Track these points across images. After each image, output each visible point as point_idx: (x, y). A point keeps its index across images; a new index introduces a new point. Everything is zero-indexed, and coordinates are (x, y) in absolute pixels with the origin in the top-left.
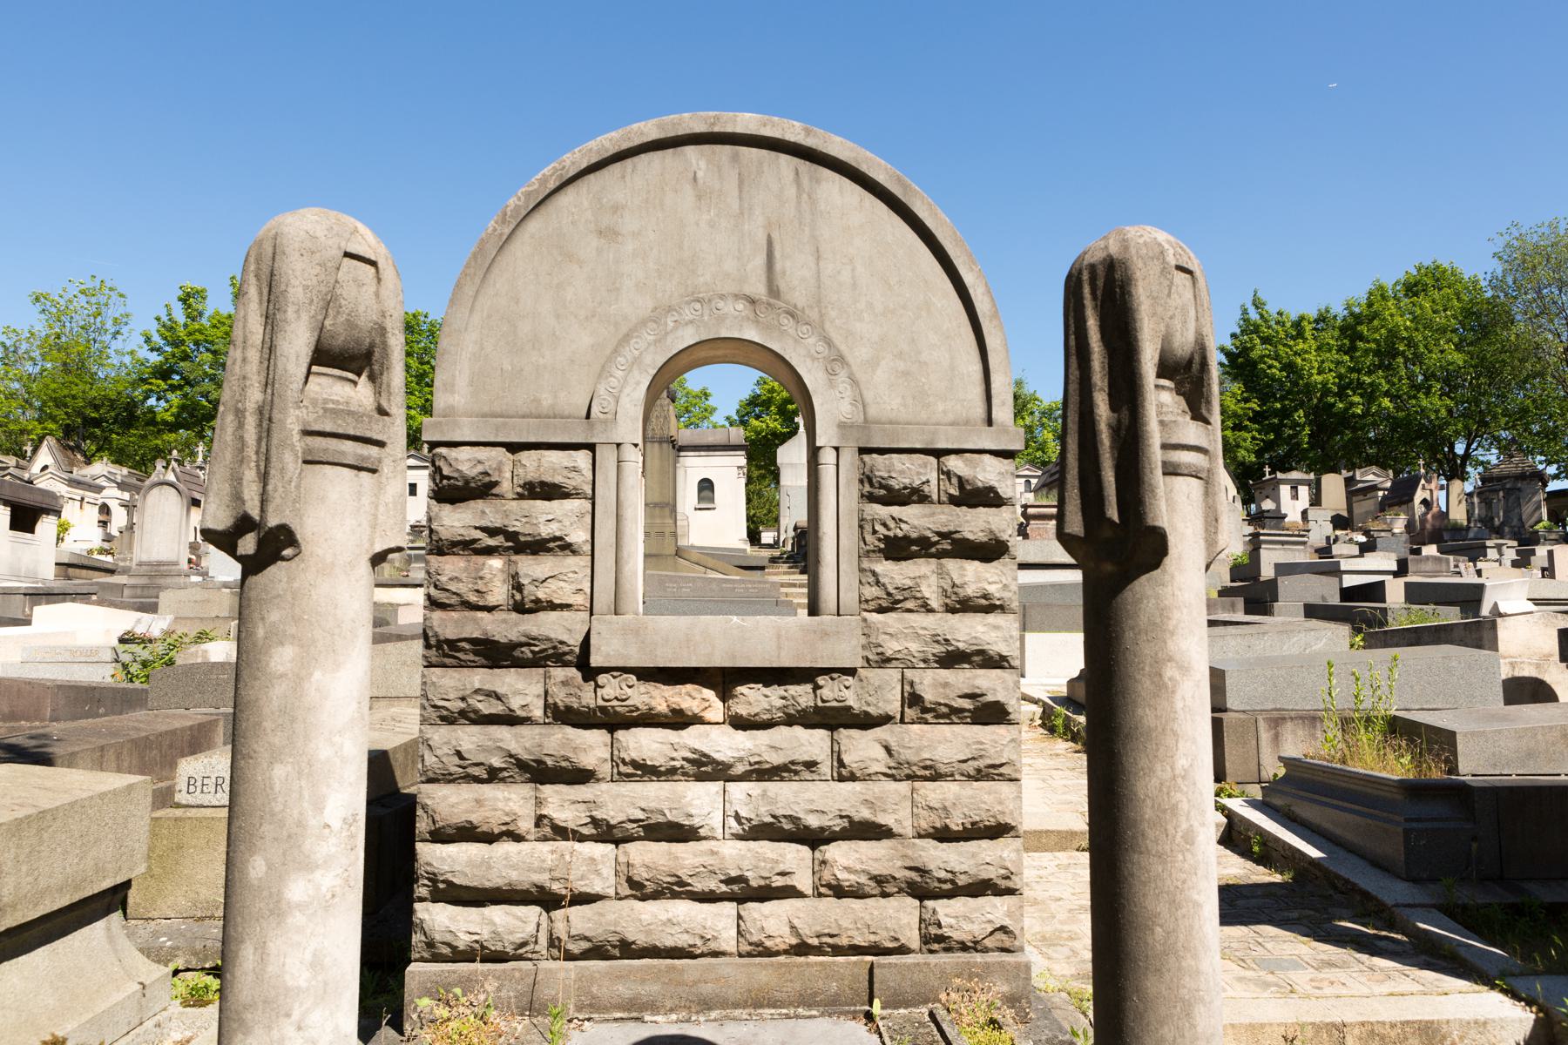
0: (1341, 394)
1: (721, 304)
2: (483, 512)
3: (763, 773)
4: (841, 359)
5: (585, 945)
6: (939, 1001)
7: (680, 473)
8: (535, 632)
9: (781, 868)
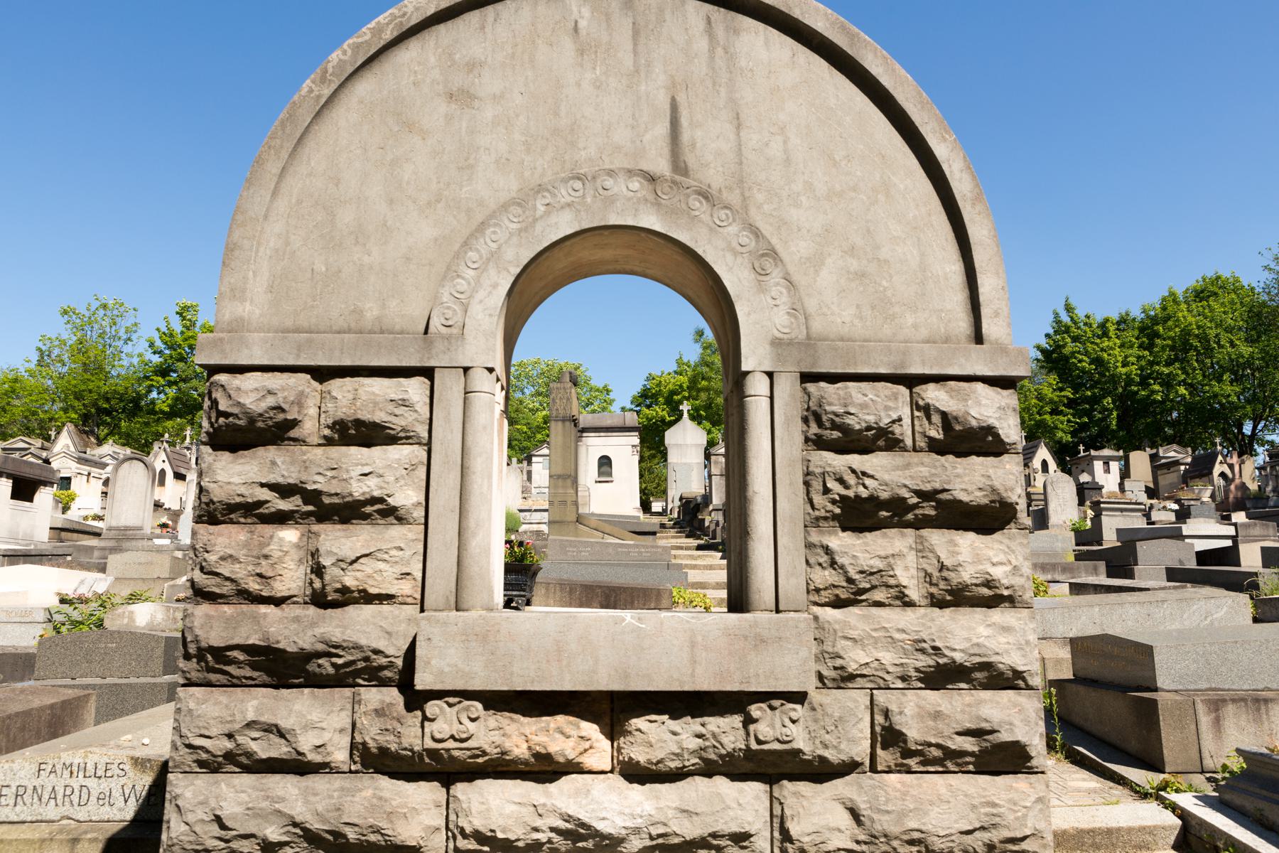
0: (1144, 382)
1: (609, 183)
2: (274, 463)
4: (773, 254)
7: (582, 450)
8: (337, 635)
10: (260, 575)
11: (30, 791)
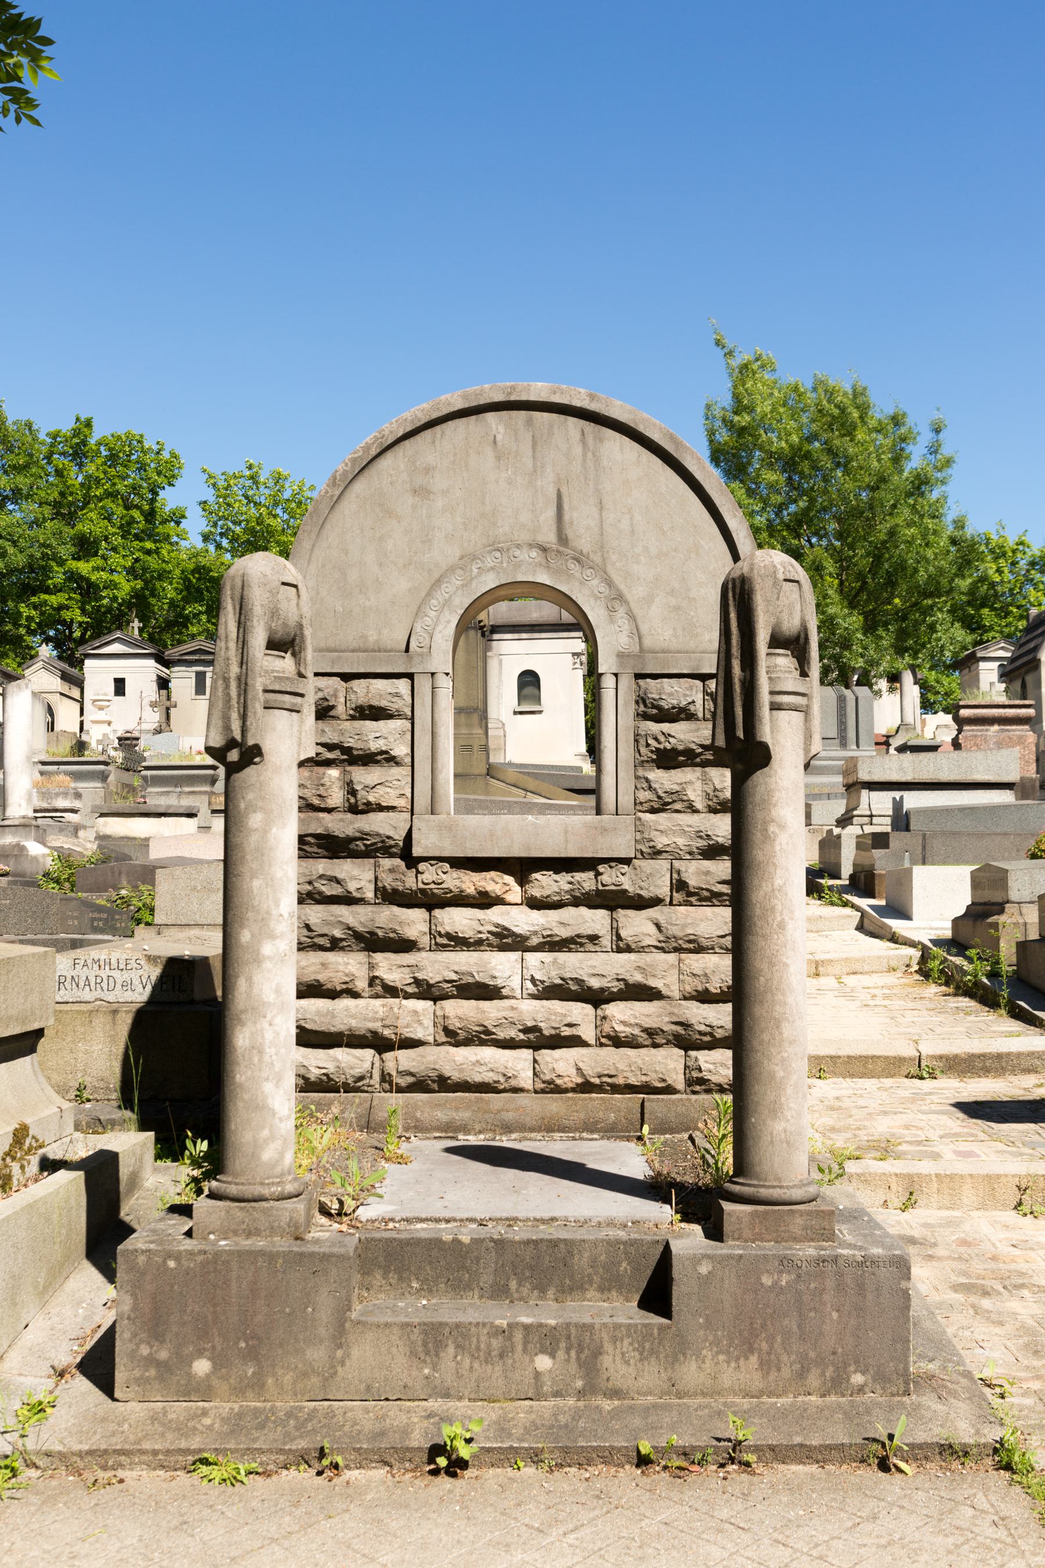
1: (517, 553)
2: (323, 731)
3: (554, 945)
4: (620, 597)
5: (410, 1080)
6: (698, 1129)
7: (493, 665)
8: (367, 828)
9: (569, 1020)
11: (69, 980)
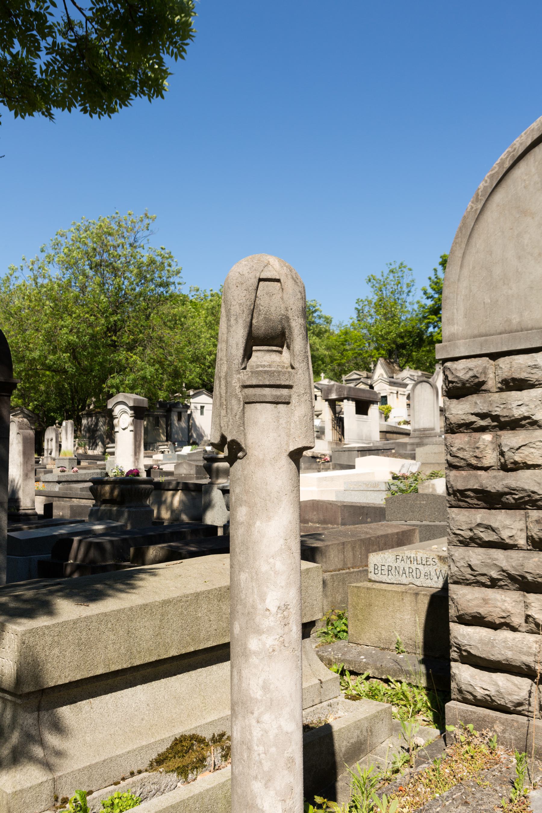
2: (476, 403)
8: (514, 485)
10: (476, 457)
11: (394, 569)
